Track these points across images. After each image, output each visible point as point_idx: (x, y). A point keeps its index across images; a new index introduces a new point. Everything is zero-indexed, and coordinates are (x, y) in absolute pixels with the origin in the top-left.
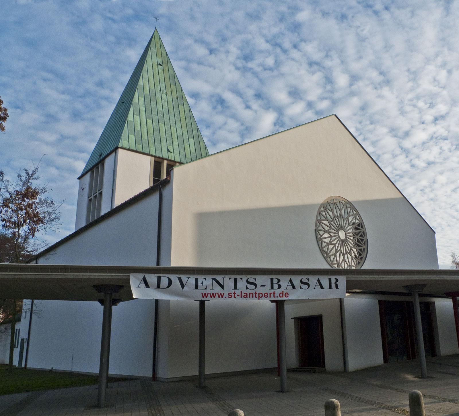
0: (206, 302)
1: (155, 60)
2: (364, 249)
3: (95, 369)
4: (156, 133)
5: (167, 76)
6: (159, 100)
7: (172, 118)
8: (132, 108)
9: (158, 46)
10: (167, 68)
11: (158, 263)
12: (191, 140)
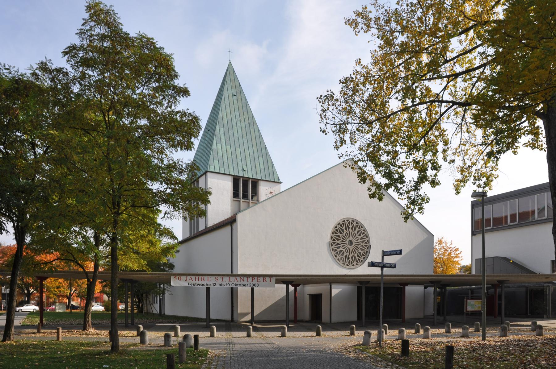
0: (246, 336)
1: (230, 92)
2: (367, 252)
3: (204, 316)
4: (234, 156)
5: (240, 104)
6: (235, 127)
7: (245, 141)
8: (215, 138)
9: (232, 78)
10: (240, 97)
11: (232, 272)
12: (261, 158)
